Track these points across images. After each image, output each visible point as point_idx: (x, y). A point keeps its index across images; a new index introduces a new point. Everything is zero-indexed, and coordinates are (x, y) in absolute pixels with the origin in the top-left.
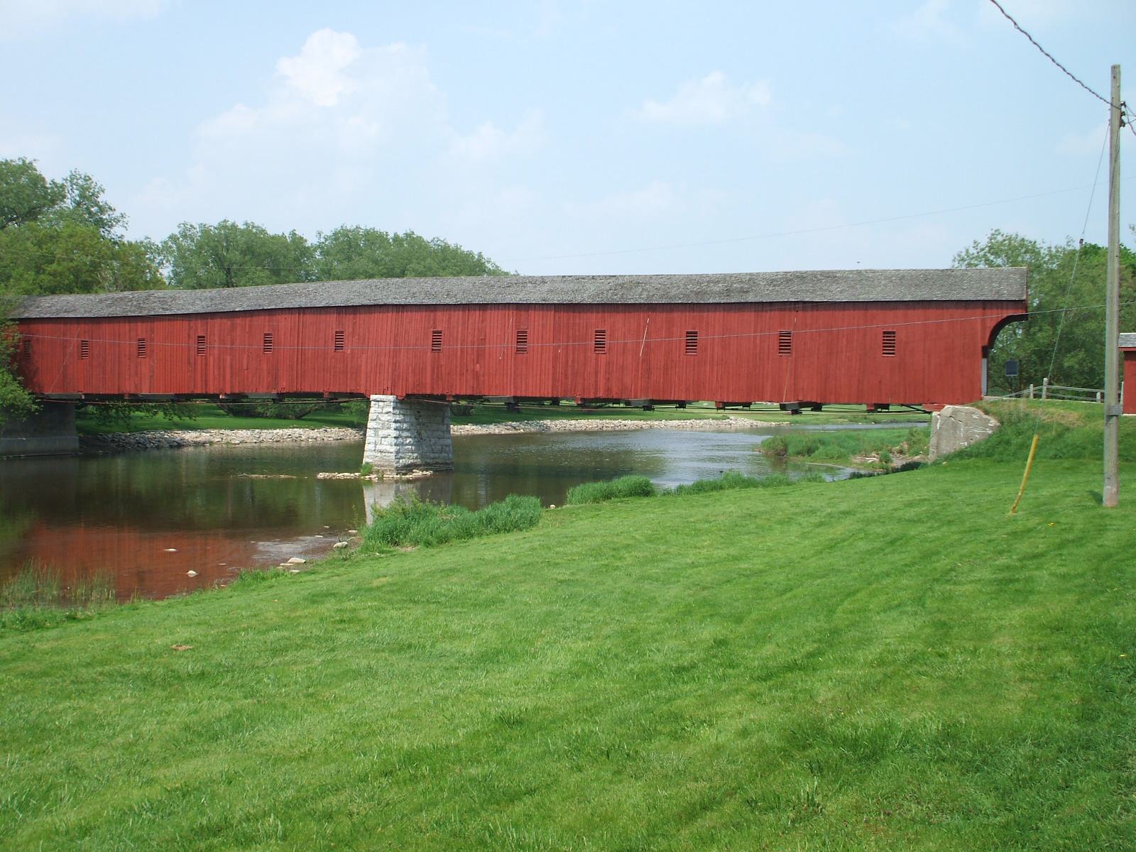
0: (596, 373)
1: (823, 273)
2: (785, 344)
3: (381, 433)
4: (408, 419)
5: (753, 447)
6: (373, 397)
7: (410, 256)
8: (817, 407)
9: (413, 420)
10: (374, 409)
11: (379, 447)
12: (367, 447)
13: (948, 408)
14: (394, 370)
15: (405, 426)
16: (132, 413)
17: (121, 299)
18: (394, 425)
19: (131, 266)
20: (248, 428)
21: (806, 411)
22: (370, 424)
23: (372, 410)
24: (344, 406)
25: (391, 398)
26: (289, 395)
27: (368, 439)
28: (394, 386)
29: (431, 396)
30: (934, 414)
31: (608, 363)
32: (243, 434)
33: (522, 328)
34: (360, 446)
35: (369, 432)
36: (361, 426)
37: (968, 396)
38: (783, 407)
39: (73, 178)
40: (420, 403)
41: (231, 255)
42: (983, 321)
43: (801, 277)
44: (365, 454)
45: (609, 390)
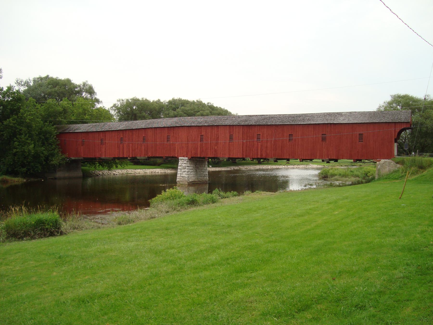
0: (257, 150)
1: (337, 113)
2: (324, 139)
3: (183, 170)
4: (192, 165)
5: (315, 176)
6: (180, 158)
7: (212, 110)
8: (336, 161)
9: (194, 166)
10: (180, 162)
11: (182, 175)
12: (178, 175)
13: (383, 161)
14: (187, 149)
15: (191, 168)
16: (5, 123)
17: (96, 125)
18: (187, 168)
19: (103, 115)
20: (141, 169)
21: (332, 162)
22: (179, 167)
23: (180, 162)
24: (172, 162)
25: (186, 158)
26: (151, 157)
27: (178, 173)
28: (187, 154)
29: (200, 158)
30: (378, 163)
31: (261, 146)
32: (139, 171)
33: (232, 133)
34: (175, 175)
35: (179, 170)
36: (176, 169)
37: (389, 156)
38: (323, 161)
39: (84, 84)
40: (196, 160)
41: (134, 110)
42: (395, 131)
43: (330, 114)
44: (177, 178)
45: (261, 155)
